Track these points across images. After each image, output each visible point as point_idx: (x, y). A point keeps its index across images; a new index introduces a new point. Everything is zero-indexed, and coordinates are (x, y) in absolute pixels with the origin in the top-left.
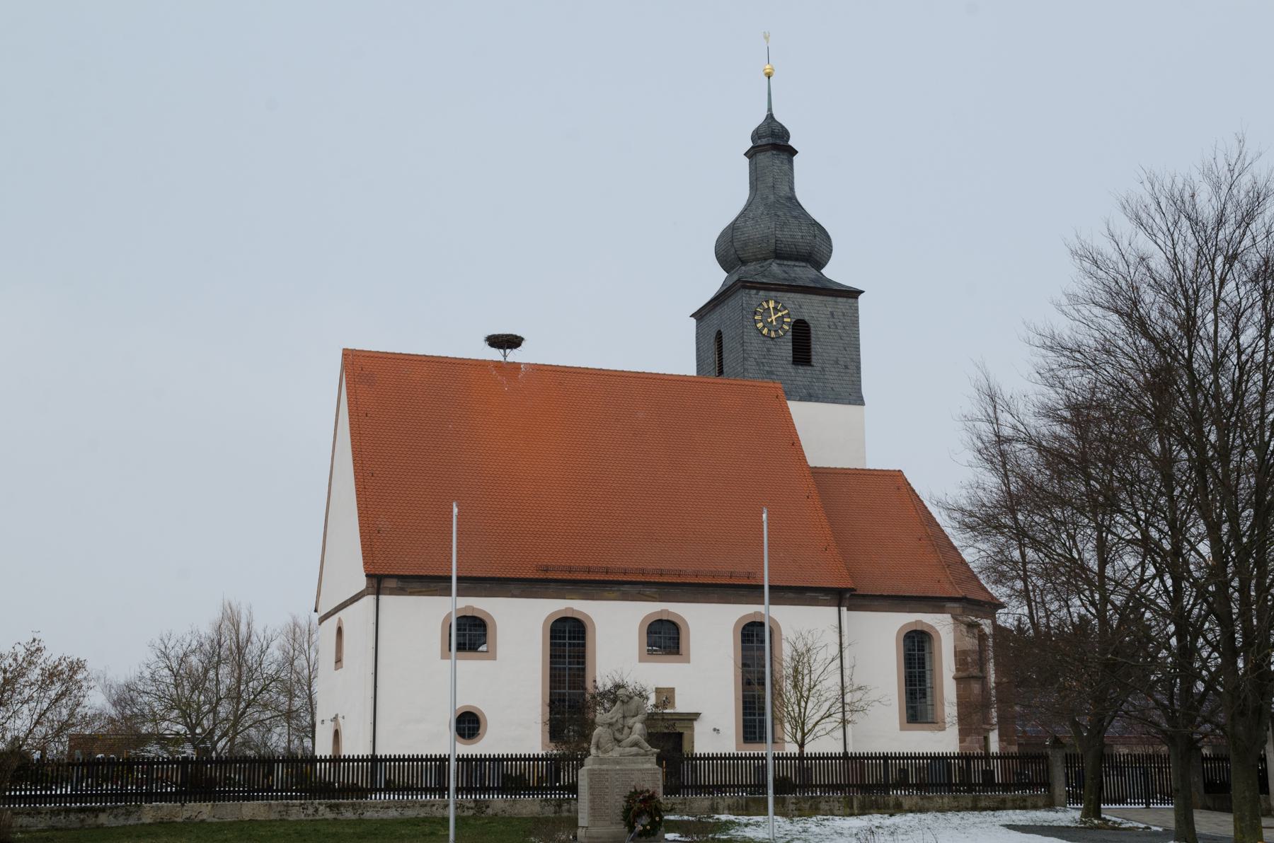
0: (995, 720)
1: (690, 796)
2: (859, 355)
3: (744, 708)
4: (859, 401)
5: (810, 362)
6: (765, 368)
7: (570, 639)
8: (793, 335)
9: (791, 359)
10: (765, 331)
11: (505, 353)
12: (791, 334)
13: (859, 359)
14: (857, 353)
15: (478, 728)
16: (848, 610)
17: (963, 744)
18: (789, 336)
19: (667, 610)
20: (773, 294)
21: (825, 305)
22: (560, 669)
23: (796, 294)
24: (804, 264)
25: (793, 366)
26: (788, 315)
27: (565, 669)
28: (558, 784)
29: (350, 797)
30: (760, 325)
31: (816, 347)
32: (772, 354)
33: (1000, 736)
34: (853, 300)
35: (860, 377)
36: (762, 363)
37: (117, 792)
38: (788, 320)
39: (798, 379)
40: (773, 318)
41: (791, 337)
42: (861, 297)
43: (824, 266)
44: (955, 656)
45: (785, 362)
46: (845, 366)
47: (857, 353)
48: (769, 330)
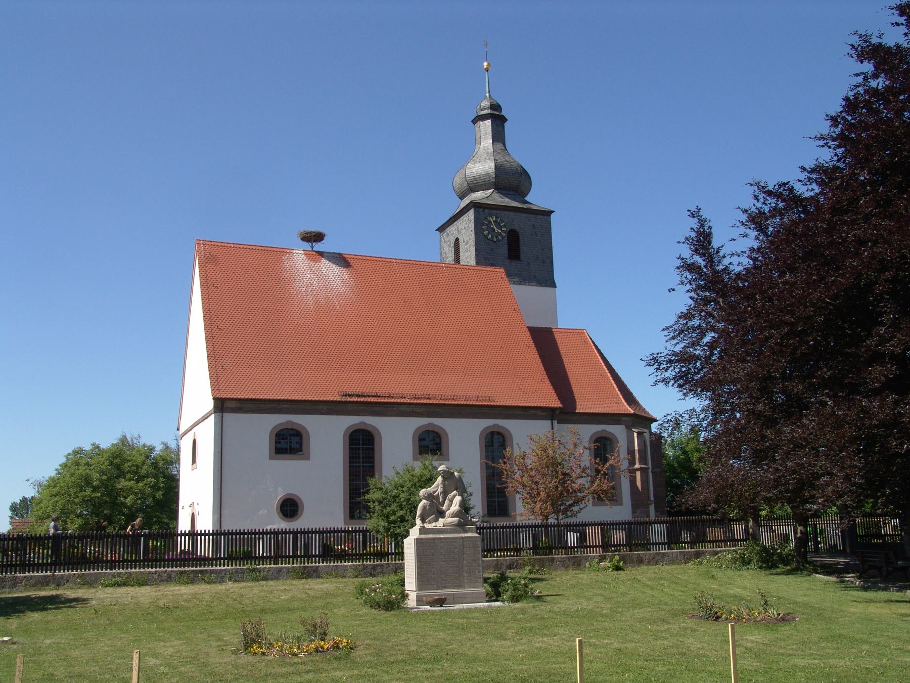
0: (652, 498)
1: (13, 573)
3: (488, 493)
4: (553, 285)
7: (363, 445)
9: (507, 256)
11: (312, 245)
12: (506, 239)
15: (297, 510)
16: (558, 423)
19: (364, 423)
20: (494, 211)
22: (356, 466)
24: (514, 193)
26: (505, 226)
27: (359, 467)
28: (365, 552)
29: (31, 570)
31: (523, 249)
33: (656, 508)
34: (548, 217)
36: (488, 258)
37: (367, 557)
38: (505, 229)
41: (507, 241)
42: (552, 215)
43: (526, 195)
48: (492, 236)
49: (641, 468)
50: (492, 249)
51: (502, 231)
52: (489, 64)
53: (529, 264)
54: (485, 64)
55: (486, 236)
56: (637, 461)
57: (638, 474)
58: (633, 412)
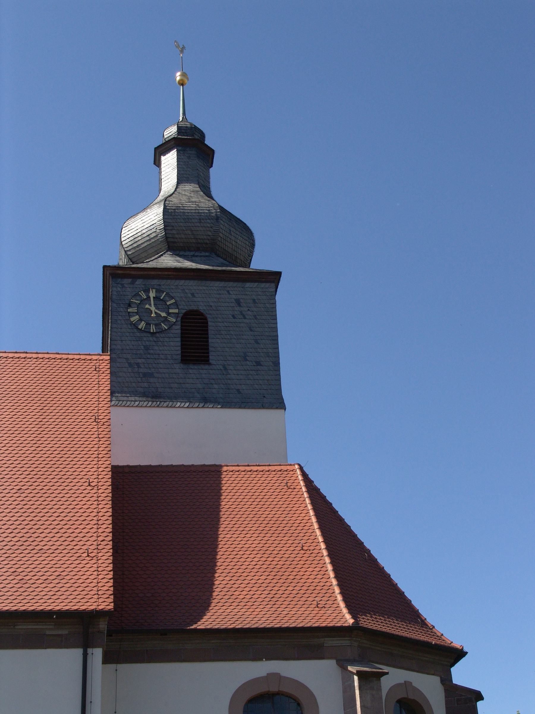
4: (280, 404)
5: (208, 361)
6: (141, 370)
8: (182, 329)
10: (153, 329)
16: (106, 660)
18: (177, 330)
19: (278, 674)
20: (155, 282)
21: (228, 292)
23: (188, 281)
24: (207, 254)
25: (182, 365)
26: (176, 305)
30: (142, 325)
32: (152, 351)
36: (138, 364)
40: (153, 308)
41: (179, 331)
46: (256, 362)
50: (147, 348)
51: (169, 314)
52: (184, 75)
53: (225, 369)
54: (178, 76)
55: (135, 325)
58: (350, 620)
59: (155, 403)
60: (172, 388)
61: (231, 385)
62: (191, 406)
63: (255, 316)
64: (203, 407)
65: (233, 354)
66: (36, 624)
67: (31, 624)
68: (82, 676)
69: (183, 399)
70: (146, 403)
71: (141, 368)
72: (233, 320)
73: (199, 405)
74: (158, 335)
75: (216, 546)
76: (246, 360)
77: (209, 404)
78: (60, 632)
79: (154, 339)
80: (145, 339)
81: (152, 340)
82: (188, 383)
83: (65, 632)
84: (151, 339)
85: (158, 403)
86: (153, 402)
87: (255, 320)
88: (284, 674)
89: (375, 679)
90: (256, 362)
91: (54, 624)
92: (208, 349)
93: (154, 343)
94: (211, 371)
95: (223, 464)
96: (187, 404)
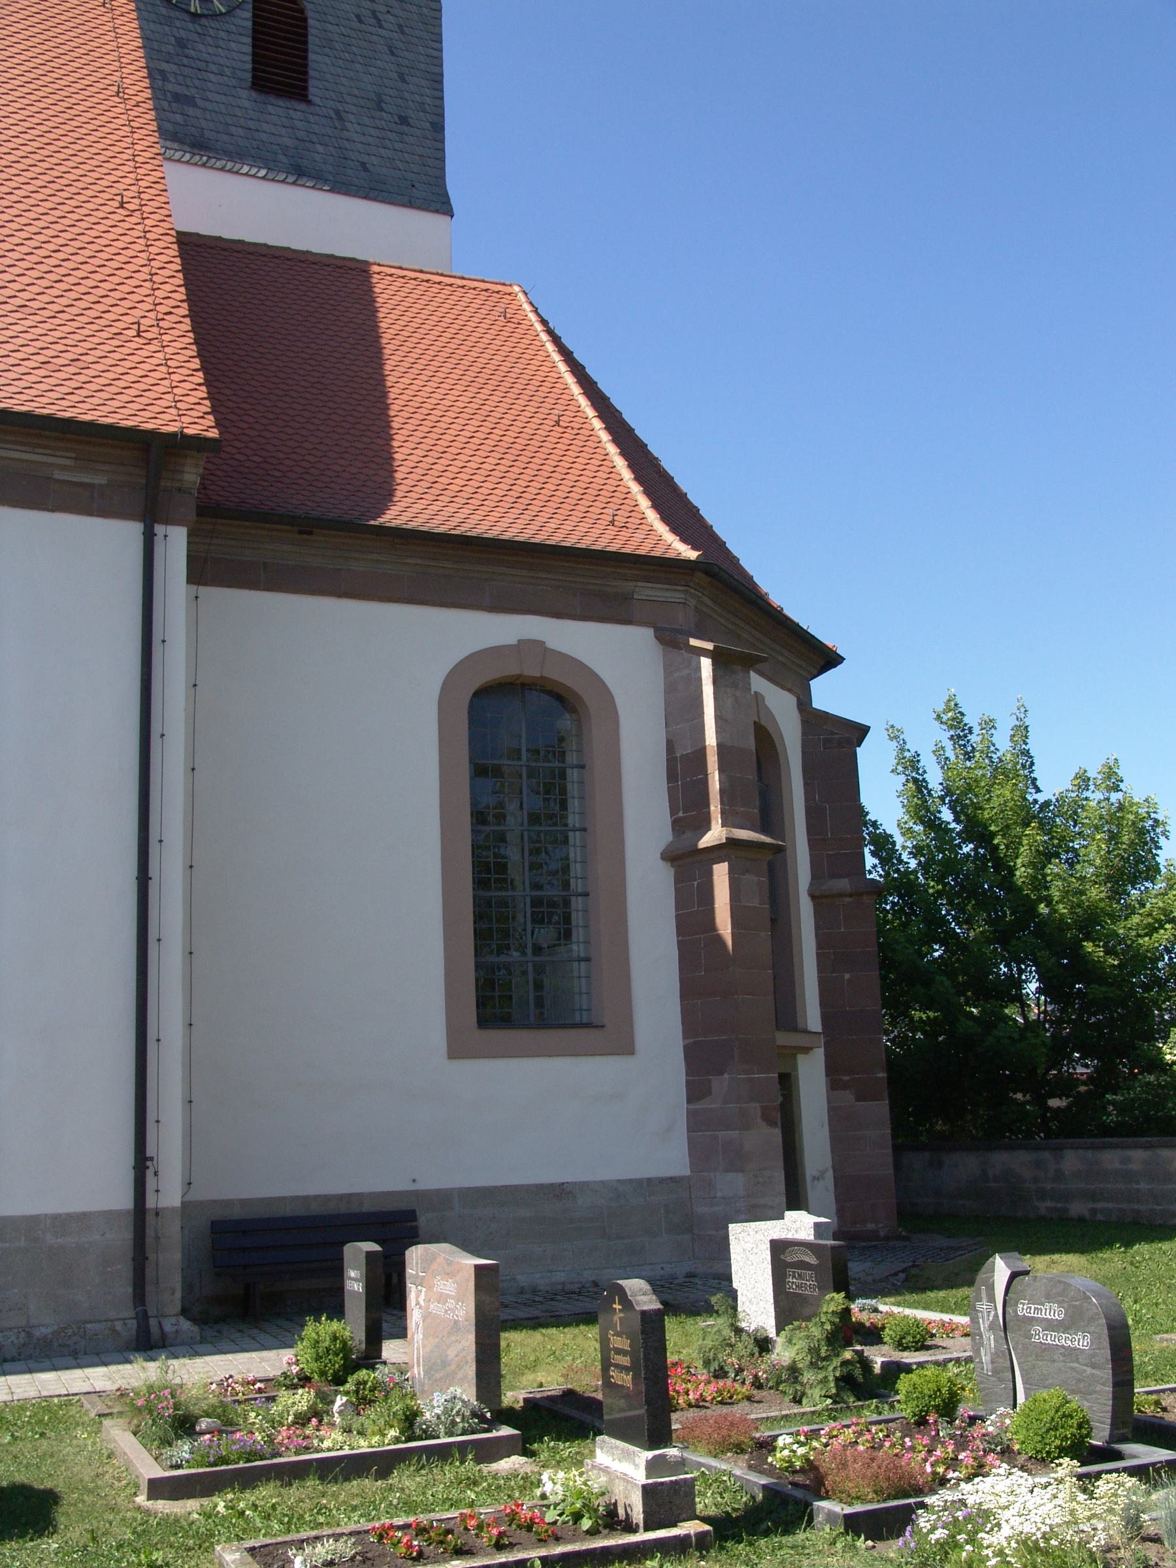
0: (813, 1019)
2: (442, 98)
4: (441, 204)
6: (169, 87)
9: (248, 76)
12: (249, 15)
13: (442, 107)
14: (437, 94)
17: (697, 1106)
25: (254, 94)
32: (192, 53)
33: (832, 1069)
35: (443, 150)
39: (265, 127)
41: (249, 24)
44: (672, 776)
45: (233, 82)
46: (400, 117)
47: (437, 94)
49: (732, 843)
50: (181, 43)
53: (341, 119)
56: (715, 808)
57: (721, 873)
59: (197, 158)
60: (232, 135)
61: (350, 153)
62: (271, 176)
63: (400, 26)
64: (294, 183)
65: (356, 92)
66: (30, 449)
67: (18, 447)
68: (141, 584)
69: (255, 161)
70: (178, 155)
71: (169, 81)
72: (356, 25)
73: (286, 177)
74: (204, 21)
75: (385, 394)
76: (382, 110)
77: (305, 179)
78: (86, 478)
79: (198, 27)
80: (178, 24)
81: (192, 29)
82: (265, 132)
83: (100, 480)
84: (190, 26)
85: (205, 158)
86: (194, 154)
87: (401, 36)
88: (552, 644)
89: (739, 668)
90: (400, 117)
91: (73, 455)
92: (306, 73)
93: (196, 37)
94: (311, 116)
95: (371, 260)
96: (263, 173)
